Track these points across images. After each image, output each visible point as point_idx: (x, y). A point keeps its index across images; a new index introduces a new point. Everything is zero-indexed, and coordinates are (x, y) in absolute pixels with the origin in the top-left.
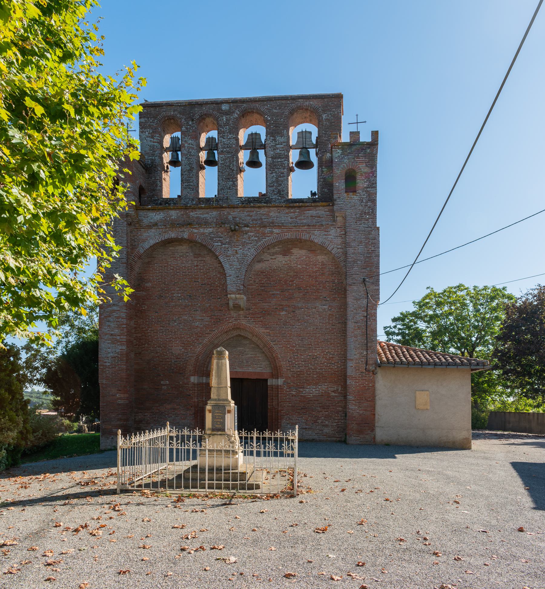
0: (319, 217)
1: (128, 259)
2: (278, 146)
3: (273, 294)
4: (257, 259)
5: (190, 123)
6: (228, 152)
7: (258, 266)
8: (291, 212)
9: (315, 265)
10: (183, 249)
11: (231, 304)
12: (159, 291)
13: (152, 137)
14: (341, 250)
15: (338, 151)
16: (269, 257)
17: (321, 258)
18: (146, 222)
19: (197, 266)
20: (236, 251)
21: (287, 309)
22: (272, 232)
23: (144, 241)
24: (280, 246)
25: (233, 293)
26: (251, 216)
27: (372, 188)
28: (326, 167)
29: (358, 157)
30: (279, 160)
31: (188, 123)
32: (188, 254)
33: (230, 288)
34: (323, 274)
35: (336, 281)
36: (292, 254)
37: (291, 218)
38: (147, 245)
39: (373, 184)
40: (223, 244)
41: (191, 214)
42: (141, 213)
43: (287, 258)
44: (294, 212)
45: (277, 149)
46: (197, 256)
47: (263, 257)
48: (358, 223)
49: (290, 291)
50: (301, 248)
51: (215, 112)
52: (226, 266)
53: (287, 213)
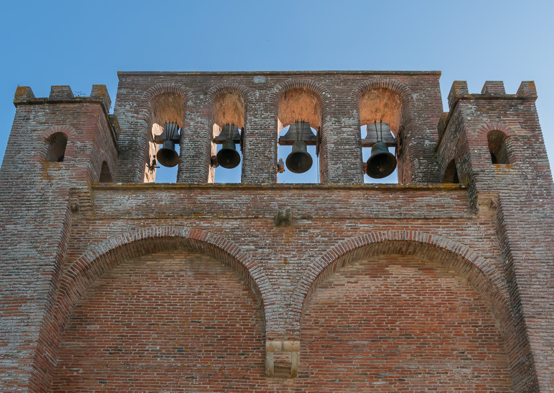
0: (443, 206)
1: (58, 269)
2: (344, 129)
3: (356, 346)
4: (320, 281)
5: (202, 97)
6: (262, 135)
7: (323, 295)
8: (390, 199)
9: (435, 294)
10: (175, 263)
11: (270, 360)
12: (114, 340)
13: (137, 112)
14: (493, 261)
15: (470, 106)
16: (343, 280)
17: (448, 281)
18: (107, 209)
19: (200, 293)
20: (285, 259)
21: (387, 374)
22: (355, 229)
23: (98, 241)
24: (365, 262)
25: (279, 337)
26: (315, 203)
27: (538, 158)
28: (424, 158)
29: (505, 115)
30: (347, 147)
31: (197, 98)
32: (182, 273)
33: (271, 326)
34: (452, 310)
35: (480, 323)
36: (387, 274)
37: (391, 207)
38: (103, 248)
39: (540, 152)
40: (258, 247)
41: (199, 198)
42: (100, 195)
43: (379, 282)
44: (395, 199)
45: (344, 132)
46: (200, 275)
47: (331, 280)
48: (526, 210)
49: (391, 341)
50: (404, 266)
51: (242, 86)
52: (265, 286)
53: (381, 200)
